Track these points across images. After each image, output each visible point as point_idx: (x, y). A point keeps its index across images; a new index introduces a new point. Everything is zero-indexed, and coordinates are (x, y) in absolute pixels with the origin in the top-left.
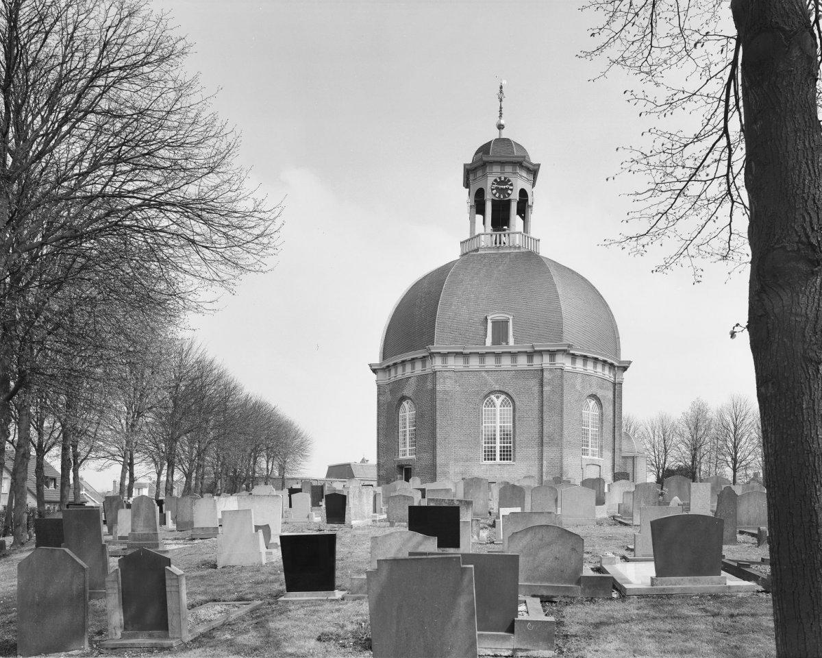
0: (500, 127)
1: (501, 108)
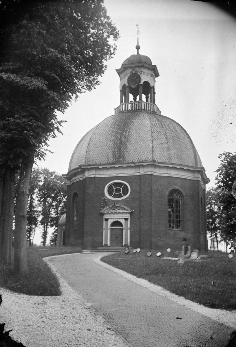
0: (138, 48)
1: (138, 38)
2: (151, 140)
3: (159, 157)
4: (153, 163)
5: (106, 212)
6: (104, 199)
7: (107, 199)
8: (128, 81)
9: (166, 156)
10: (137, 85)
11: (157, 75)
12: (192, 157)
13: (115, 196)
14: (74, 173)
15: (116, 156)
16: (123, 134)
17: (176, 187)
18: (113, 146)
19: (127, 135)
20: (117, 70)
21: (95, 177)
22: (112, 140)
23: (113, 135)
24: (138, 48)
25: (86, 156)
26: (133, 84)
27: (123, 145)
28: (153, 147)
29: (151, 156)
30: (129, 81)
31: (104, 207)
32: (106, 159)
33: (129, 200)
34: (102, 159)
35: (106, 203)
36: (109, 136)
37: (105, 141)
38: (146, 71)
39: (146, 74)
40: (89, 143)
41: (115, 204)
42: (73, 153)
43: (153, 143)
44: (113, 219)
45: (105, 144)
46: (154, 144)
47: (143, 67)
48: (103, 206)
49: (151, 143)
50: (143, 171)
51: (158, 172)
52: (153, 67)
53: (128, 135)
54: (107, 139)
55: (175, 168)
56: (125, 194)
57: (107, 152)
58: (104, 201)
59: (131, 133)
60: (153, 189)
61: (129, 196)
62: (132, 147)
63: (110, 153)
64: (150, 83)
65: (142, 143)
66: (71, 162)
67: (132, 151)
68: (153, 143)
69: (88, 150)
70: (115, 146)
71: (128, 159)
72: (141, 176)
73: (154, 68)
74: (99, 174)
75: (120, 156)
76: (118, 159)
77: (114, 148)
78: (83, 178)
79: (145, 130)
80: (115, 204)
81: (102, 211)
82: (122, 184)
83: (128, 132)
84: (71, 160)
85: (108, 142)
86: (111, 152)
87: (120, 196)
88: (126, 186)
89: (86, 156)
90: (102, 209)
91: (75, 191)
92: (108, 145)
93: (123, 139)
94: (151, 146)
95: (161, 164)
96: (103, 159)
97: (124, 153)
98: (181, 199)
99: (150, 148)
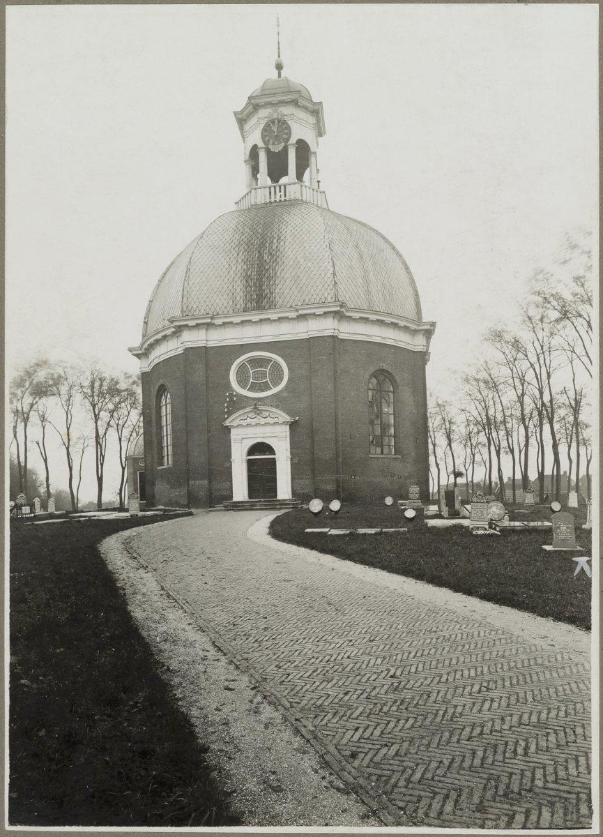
0: (279, 67)
1: (279, 43)
2: (330, 256)
3: (347, 297)
4: (338, 309)
5: (236, 425)
6: (231, 394)
7: (239, 395)
8: (263, 137)
9: (362, 295)
10: (283, 145)
11: (320, 135)
12: (411, 300)
13: (253, 388)
14: (178, 514)
15: (251, 296)
16: (264, 245)
17: (385, 367)
18: (244, 274)
19: (274, 248)
20: (235, 113)
21: (208, 346)
22: (240, 260)
23: (241, 248)
24: (279, 67)
25: (183, 298)
26: (273, 144)
27: (268, 270)
28: (334, 274)
29: (332, 294)
30: (266, 137)
31: (230, 413)
32: (231, 303)
33: (285, 394)
34: (220, 305)
35: (237, 403)
36: (233, 252)
37: (225, 263)
38: (301, 114)
39: (301, 121)
40: (188, 269)
41: (255, 405)
42: (150, 301)
43: (334, 266)
44: (252, 440)
45: (224, 270)
46: (337, 268)
47: (295, 103)
48: (228, 410)
49: (331, 264)
50: (326, 327)
51: (347, 331)
52: (316, 107)
53: (277, 247)
54: (228, 259)
55: (381, 323)
56: (276, 384)
57: (230, 287)
58: (232, 400)
59: (282, 243)
60: (338, 370)
61: (287, 386)
62: (288, 275)
63: (238, 290)
64: (310, 145)
65: (309, 264)
66: (146, 321)
67: (287, 283)
68: (334, 266)
69: (186, 284)
70: (249, 273)
71: (280, 301)
72: (311, 340)
73: (318, 110)
74: (216, 338)
75: (262, 296)
76: (257, 303)
77: (247, 278)
78: (179, 350)
79: (317, 226)
80: (255, 405)
81: (227, 423)
82: (268, 361)
83: (275, 241)
84: (147, 317)
85: (232, 265)
86: (239, 287)
87: (265, 387)
88: (277, 365)
89: (183, 298)
90: (227, 418)
91: (161, 382)
92: (232, 272)
93: (266, 257)
94: (331, 271)
95: (354, 312)
96: (220, 303)
97: (270, 290)
98: (391, 392)
99: (329, 275)
